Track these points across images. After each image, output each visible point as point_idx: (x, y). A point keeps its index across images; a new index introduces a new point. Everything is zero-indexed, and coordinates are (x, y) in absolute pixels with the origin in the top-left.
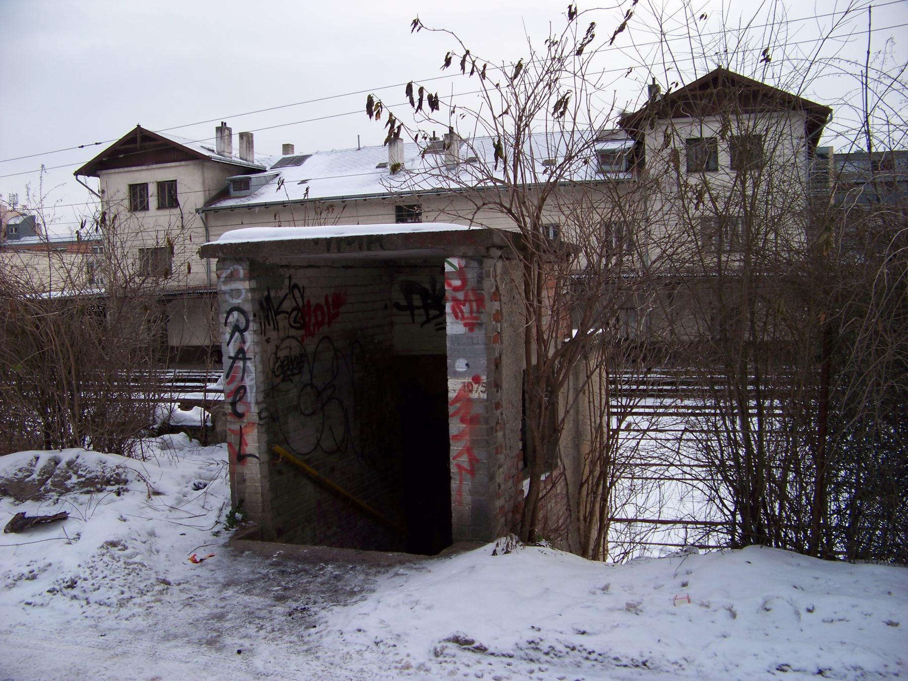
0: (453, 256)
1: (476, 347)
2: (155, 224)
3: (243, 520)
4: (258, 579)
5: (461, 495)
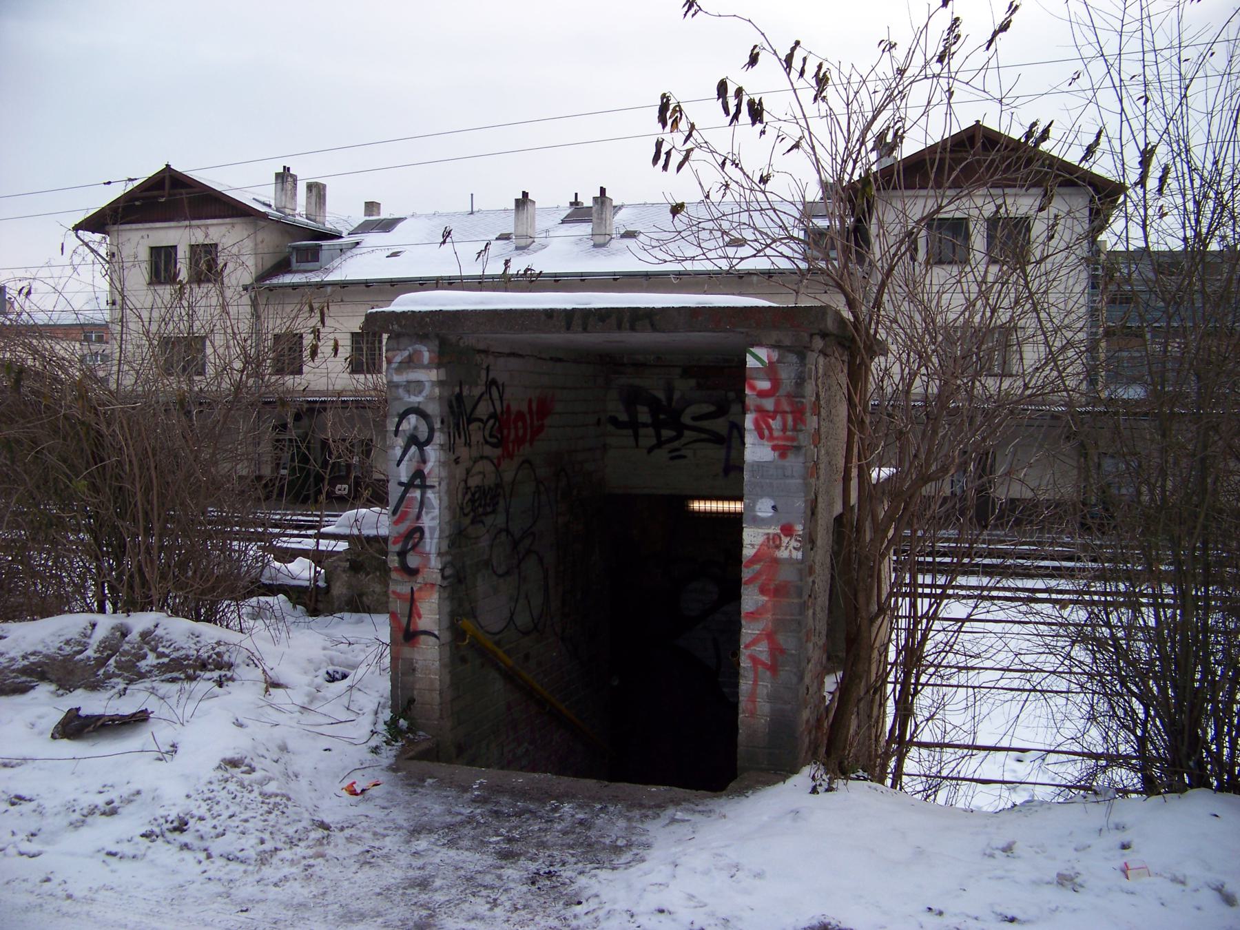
0: (760, 345)
1: (788, 481)
3: (410, 729)
4: (462, 823)
5: (754, 702)
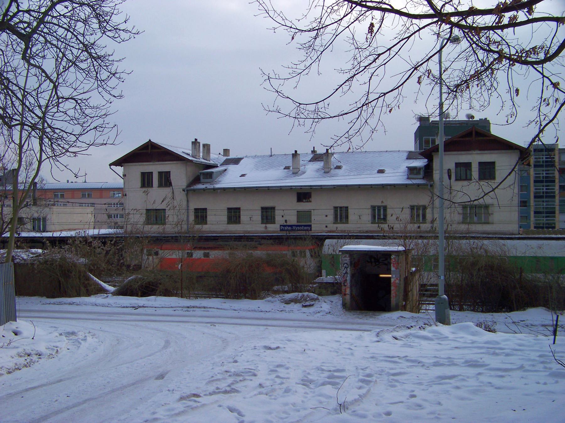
2: (157, 196)
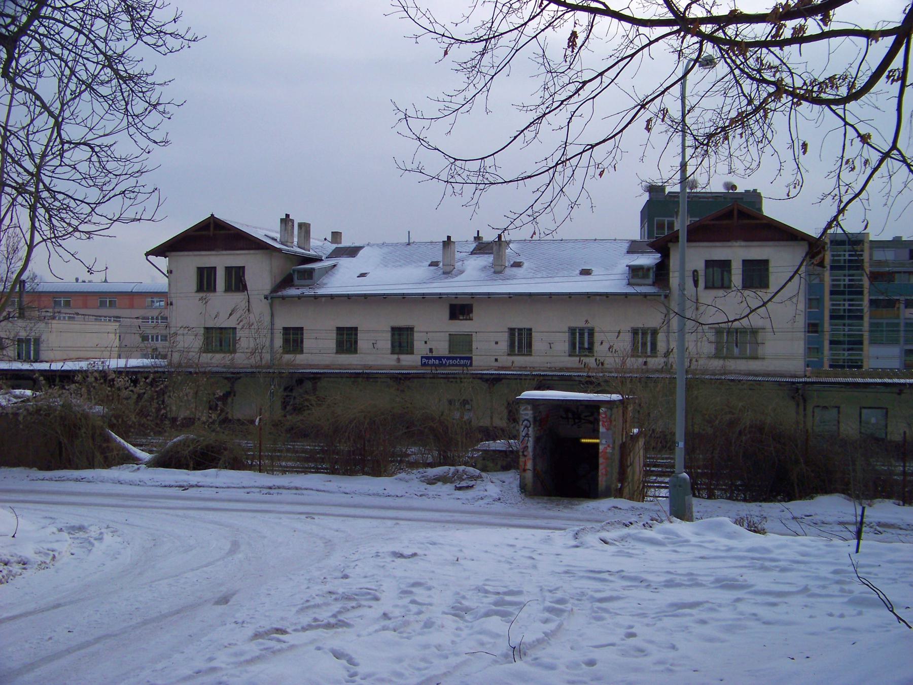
2: (222, 307)
